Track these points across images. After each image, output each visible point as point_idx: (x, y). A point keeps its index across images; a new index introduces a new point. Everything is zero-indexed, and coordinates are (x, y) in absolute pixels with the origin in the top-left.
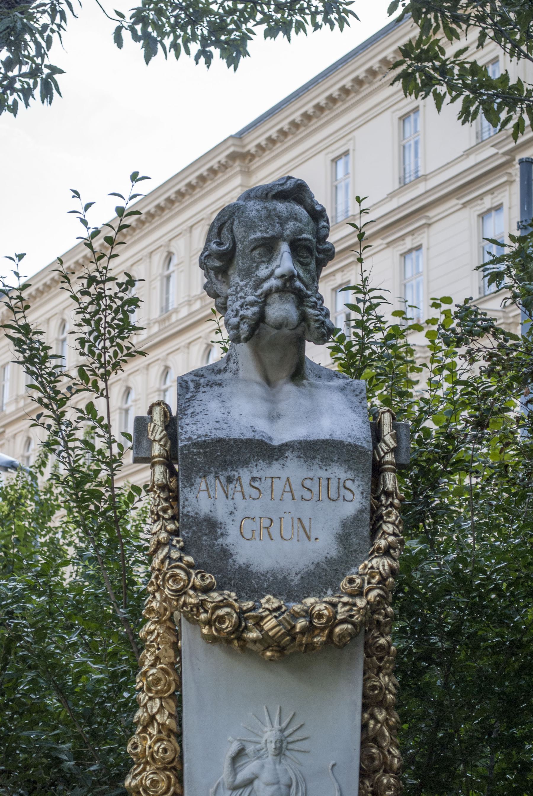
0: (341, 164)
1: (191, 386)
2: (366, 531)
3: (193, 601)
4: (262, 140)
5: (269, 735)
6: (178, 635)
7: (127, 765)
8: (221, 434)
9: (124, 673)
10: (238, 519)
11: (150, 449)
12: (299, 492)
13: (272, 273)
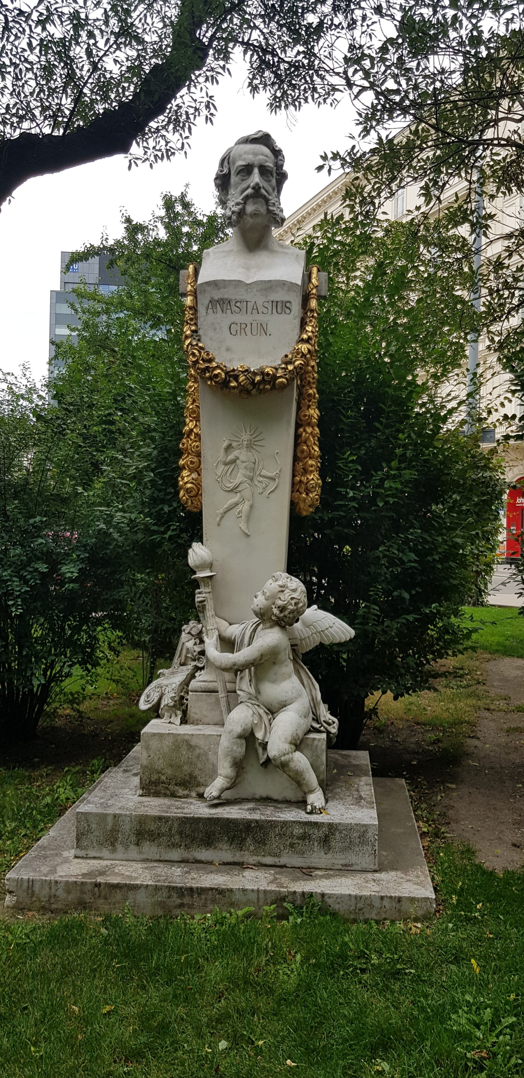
3: (203, 367)
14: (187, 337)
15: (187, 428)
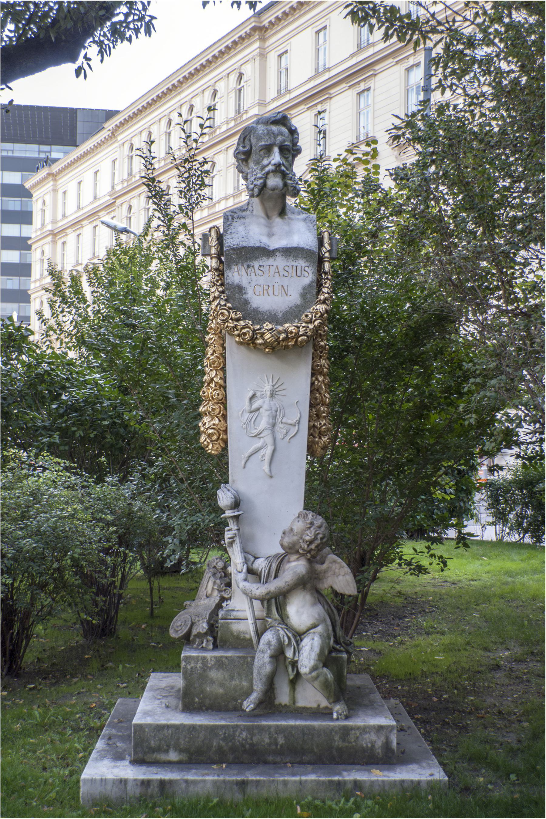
0: (321, 34)
1: (231, 217)
2: (314, 292)
3: (231, 325)
4: (272, 18)
5: (267, 388)
6: (224, 341)
7: (200, 401)
8: (245, 244)
9: (200, 356)
10: (253, 286)
11: (210, 250)
12: (282, 272)
13: (270, 163)
15: (206, 377)
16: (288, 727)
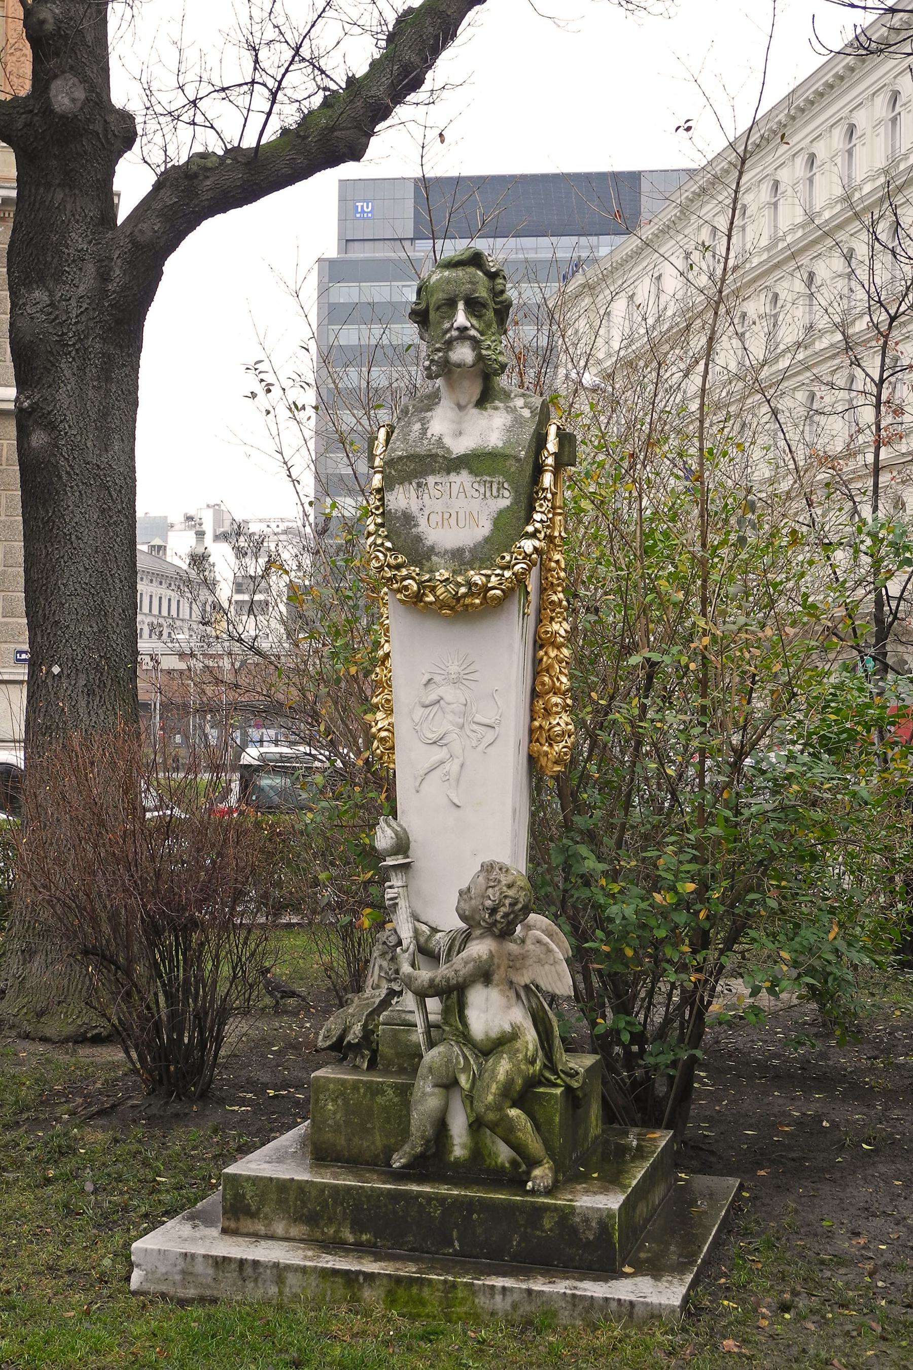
3: (389, 575)
10: (426, 513)
14: (370, 534)
16: (420, 1194)
